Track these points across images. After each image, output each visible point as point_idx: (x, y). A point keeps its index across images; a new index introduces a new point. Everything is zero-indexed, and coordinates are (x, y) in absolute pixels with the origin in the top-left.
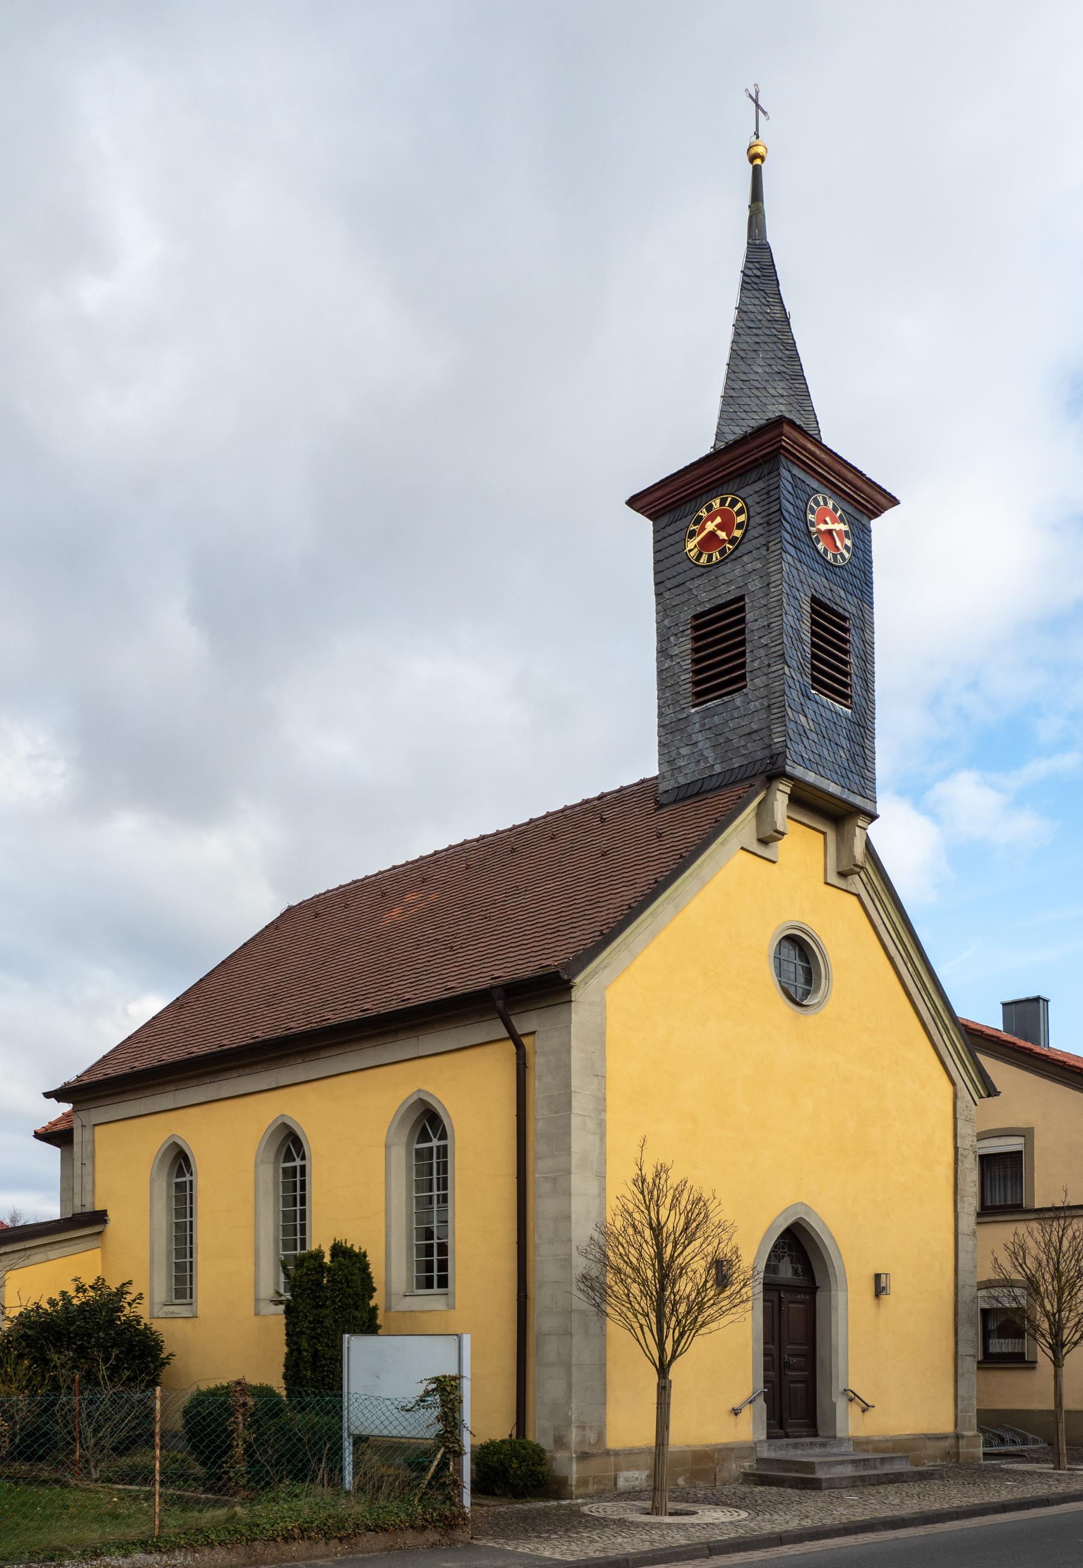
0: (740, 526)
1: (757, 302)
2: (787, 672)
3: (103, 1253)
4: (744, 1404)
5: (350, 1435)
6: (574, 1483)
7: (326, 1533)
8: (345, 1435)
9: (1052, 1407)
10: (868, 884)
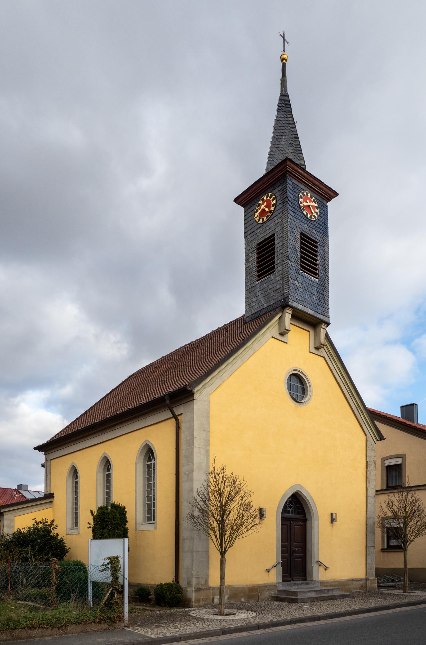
0: (273, 205)
1: (283, 116)
2: (290, 264)
3: (53, 509)
4: (272, 568)
5: (91, 582)
6: (194, 601)
7: (51, 625)
8: (89, 581)
9: (403, 567)
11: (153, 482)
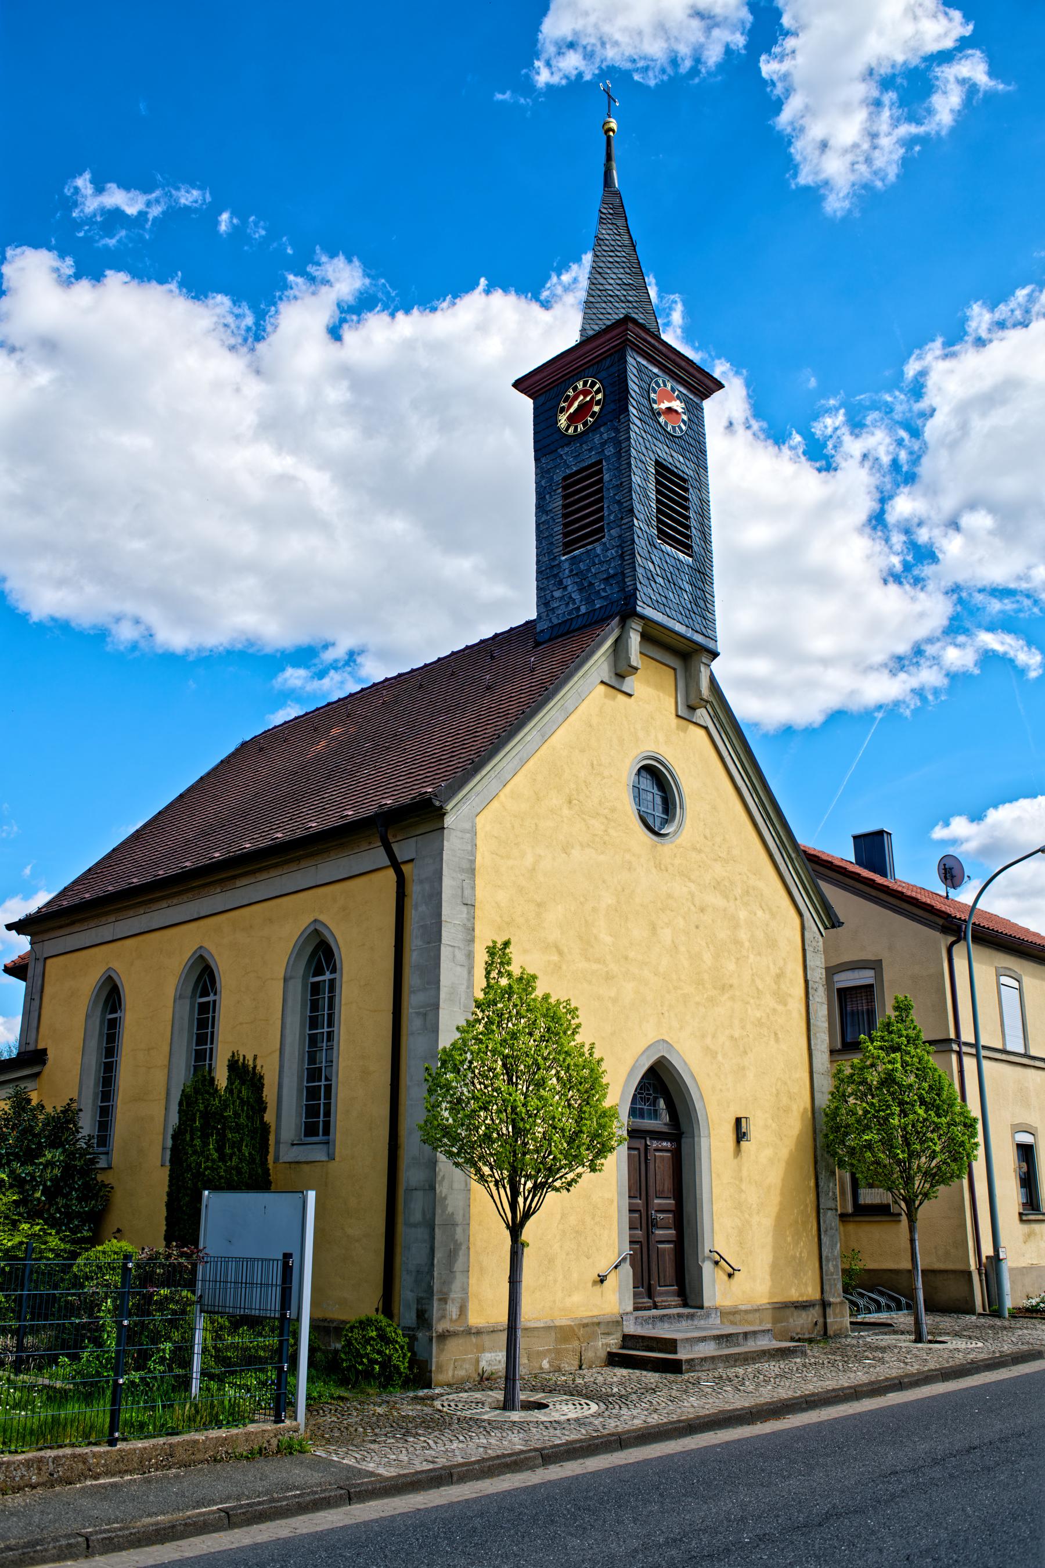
10: (715, 717)
11: (326, 1030)
